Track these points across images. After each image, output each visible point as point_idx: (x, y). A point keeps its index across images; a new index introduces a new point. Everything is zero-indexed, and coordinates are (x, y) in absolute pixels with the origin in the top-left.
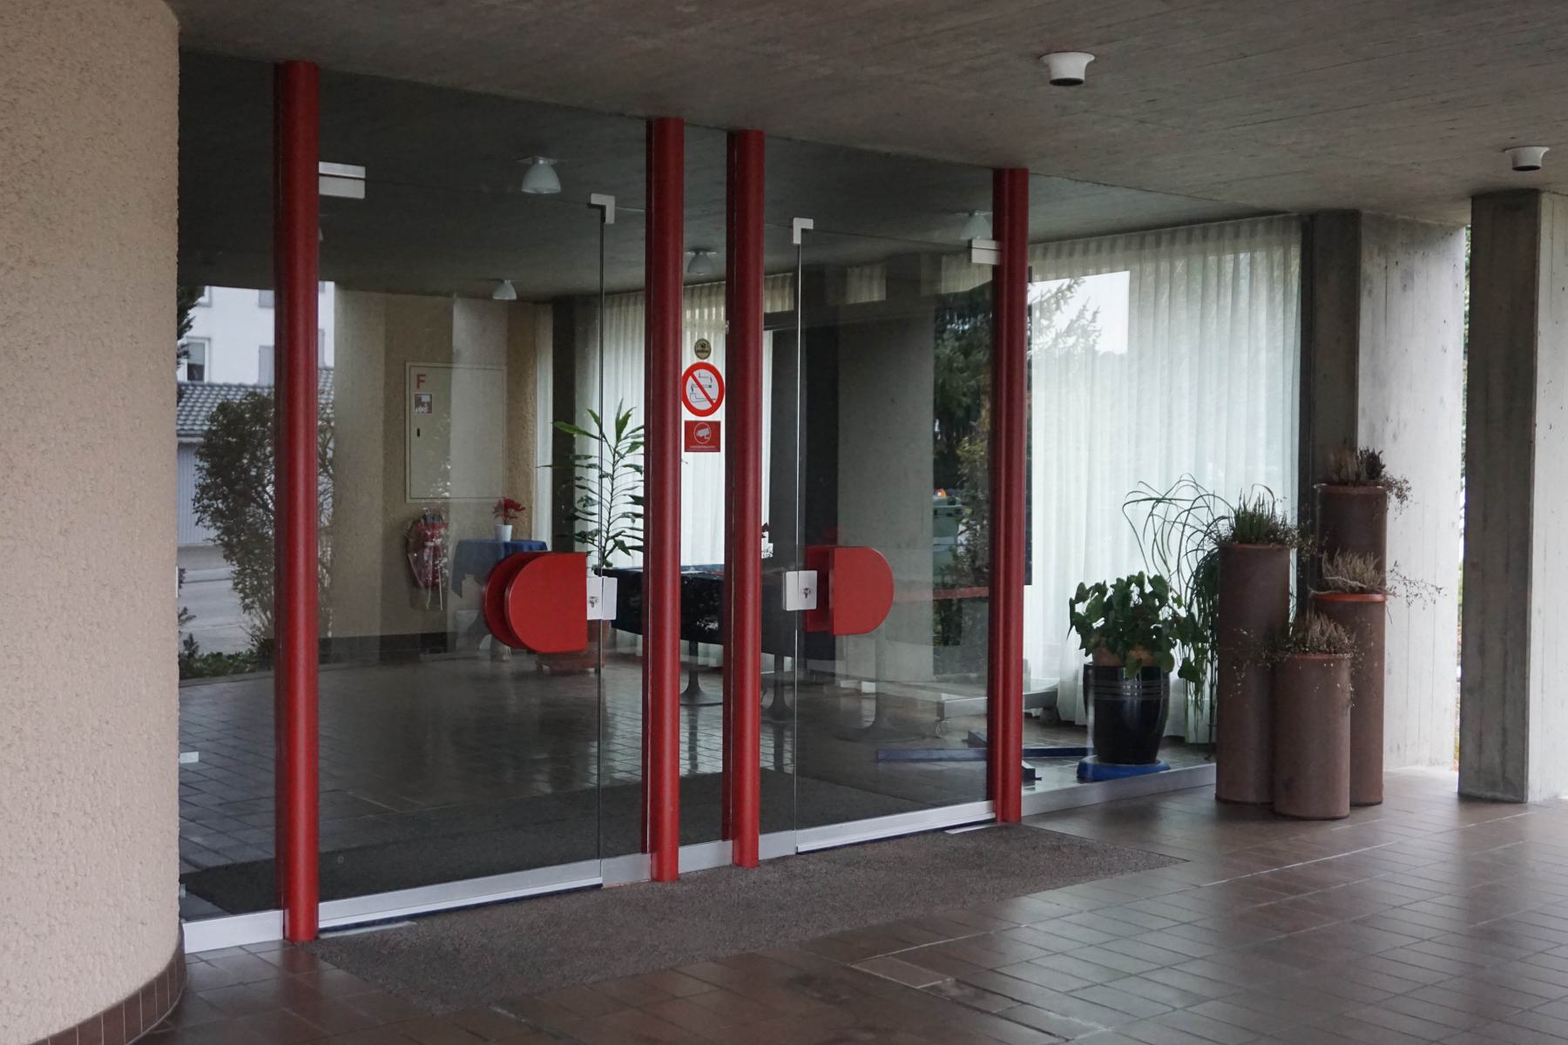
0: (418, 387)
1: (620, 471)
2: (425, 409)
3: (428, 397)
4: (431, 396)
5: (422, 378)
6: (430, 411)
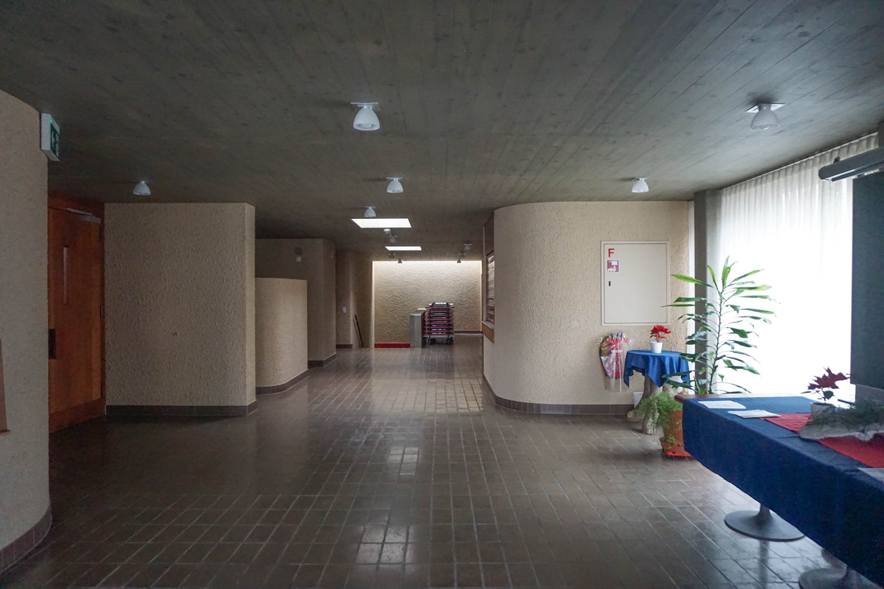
0: (609, 256)
1: (724, 309)
2: (614, 269)
3: (617, 262)
4: (618, 261)
5: (611, 251)
6: (617, 271)
